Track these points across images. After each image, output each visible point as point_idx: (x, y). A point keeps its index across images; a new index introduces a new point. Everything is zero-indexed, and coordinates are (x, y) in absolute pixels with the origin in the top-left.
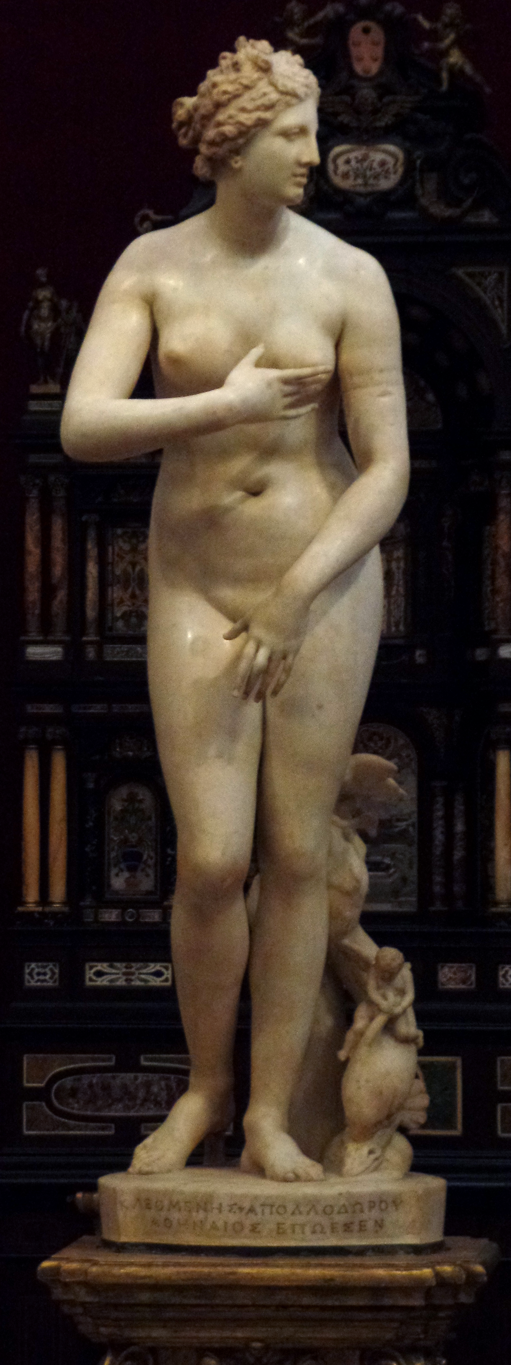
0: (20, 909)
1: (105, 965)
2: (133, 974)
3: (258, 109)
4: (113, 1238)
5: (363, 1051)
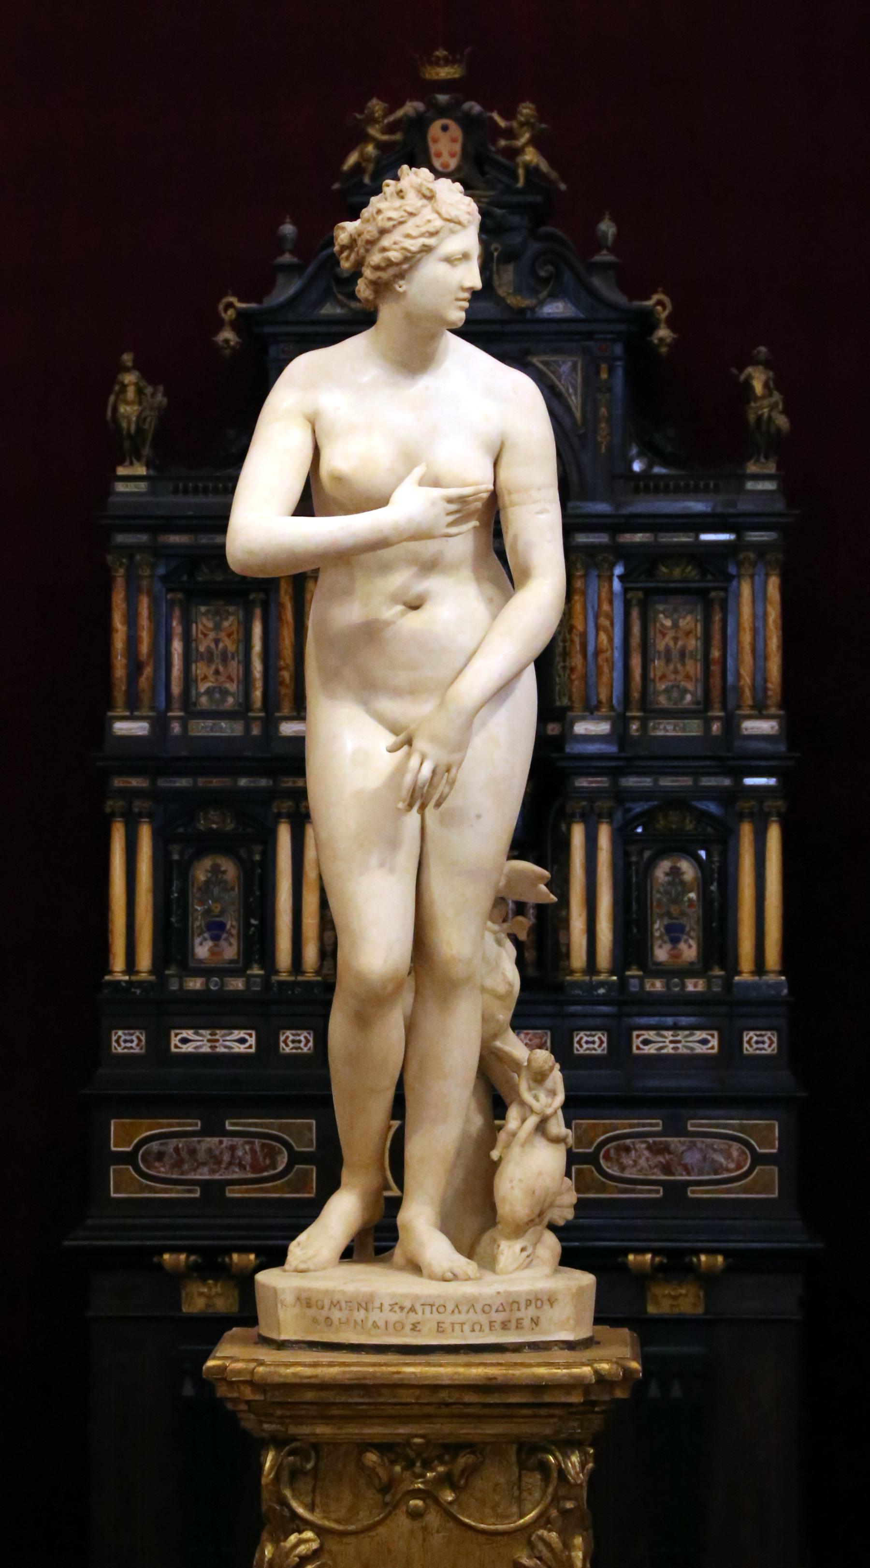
0: (107, 978)
1: (190, 1032)
2: (217, 1041)
3: (422, 235)
4: (274, 1336)
5: (516, 1150)
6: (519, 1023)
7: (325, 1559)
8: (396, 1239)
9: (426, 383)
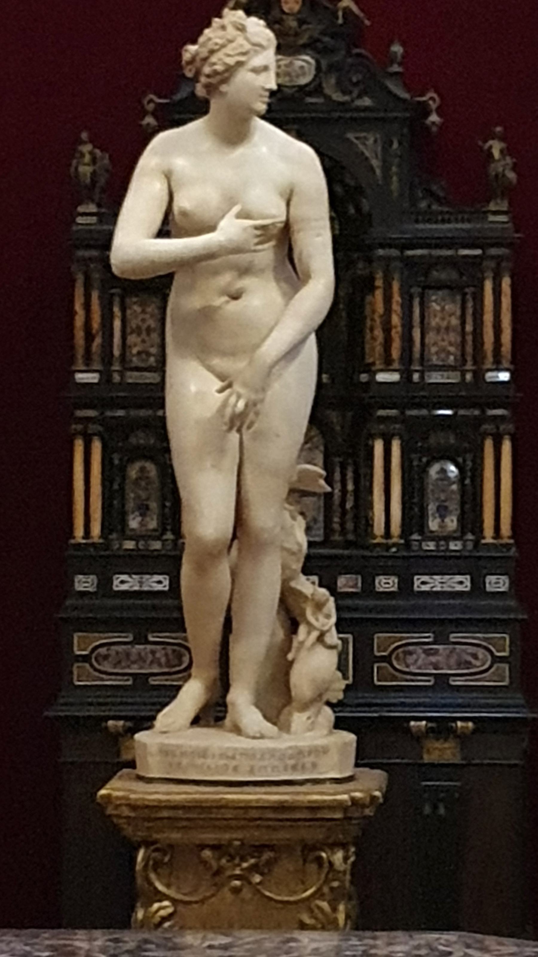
5: (303, 654)
6: (306, 571)
7: (176, 919)
8: (226, 712)
9: (240, 151)
